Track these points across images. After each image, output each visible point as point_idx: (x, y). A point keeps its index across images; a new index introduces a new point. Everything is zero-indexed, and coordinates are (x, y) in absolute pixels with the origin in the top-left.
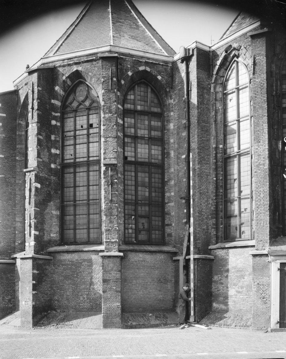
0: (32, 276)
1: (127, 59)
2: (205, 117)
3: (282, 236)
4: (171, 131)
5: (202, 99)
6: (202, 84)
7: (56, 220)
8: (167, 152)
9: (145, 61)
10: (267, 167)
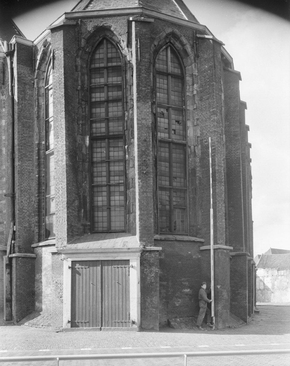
2: (28, 113)
3: (89, 234)
6: (23, 80)
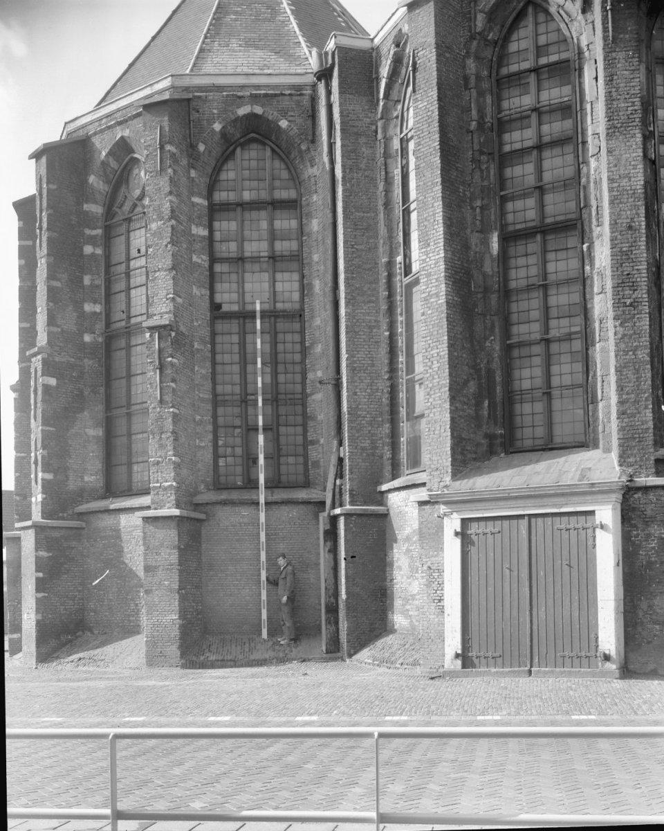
0: (34, 564)
1: (211, 98)
2: (364, 197)
4: (314, 237)
5: (356, 159)
6: (353, 126)
7: (96, 447)
8: (308, 284)
9: (251, 94)
10: (443, 301)
